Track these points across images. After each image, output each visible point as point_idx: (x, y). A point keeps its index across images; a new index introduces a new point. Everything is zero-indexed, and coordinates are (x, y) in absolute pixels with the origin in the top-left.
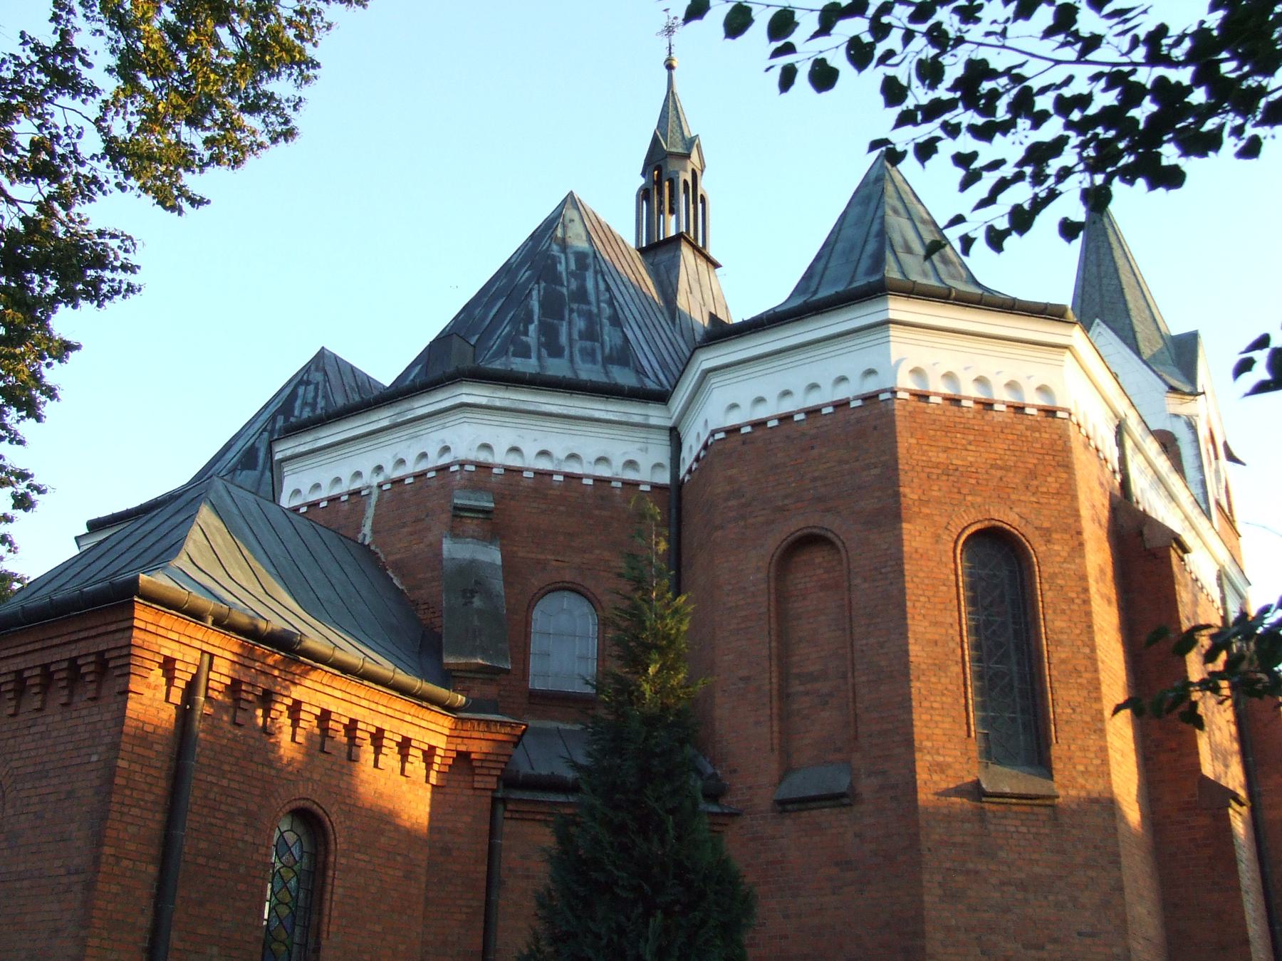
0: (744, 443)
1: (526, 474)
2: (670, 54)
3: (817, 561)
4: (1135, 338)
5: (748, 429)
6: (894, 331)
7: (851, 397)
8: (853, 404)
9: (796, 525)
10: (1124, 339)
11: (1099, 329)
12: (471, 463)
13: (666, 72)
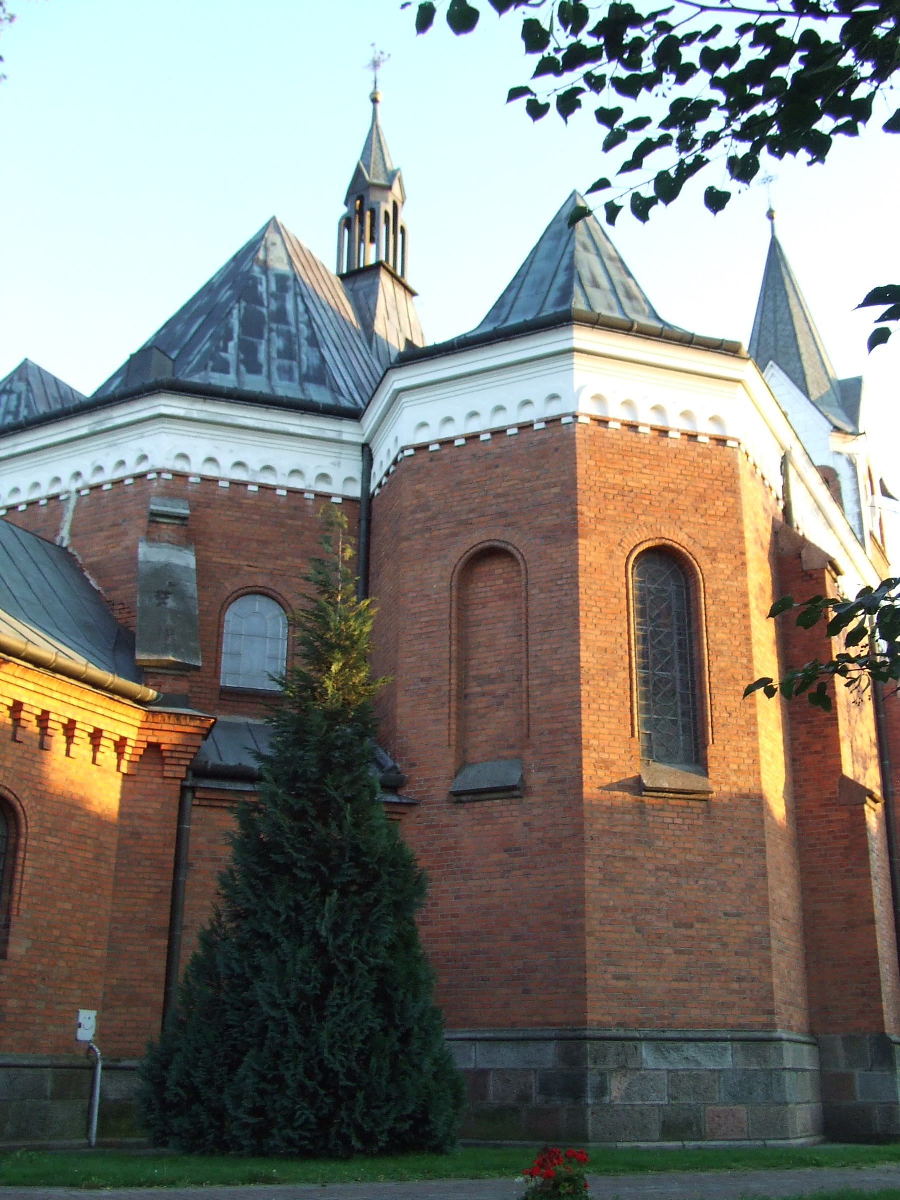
2: (376, 87)
4: (805, 379)
6: (578, 359)
7: (535, 420)
10: (795, 381)
11: (772, 371)
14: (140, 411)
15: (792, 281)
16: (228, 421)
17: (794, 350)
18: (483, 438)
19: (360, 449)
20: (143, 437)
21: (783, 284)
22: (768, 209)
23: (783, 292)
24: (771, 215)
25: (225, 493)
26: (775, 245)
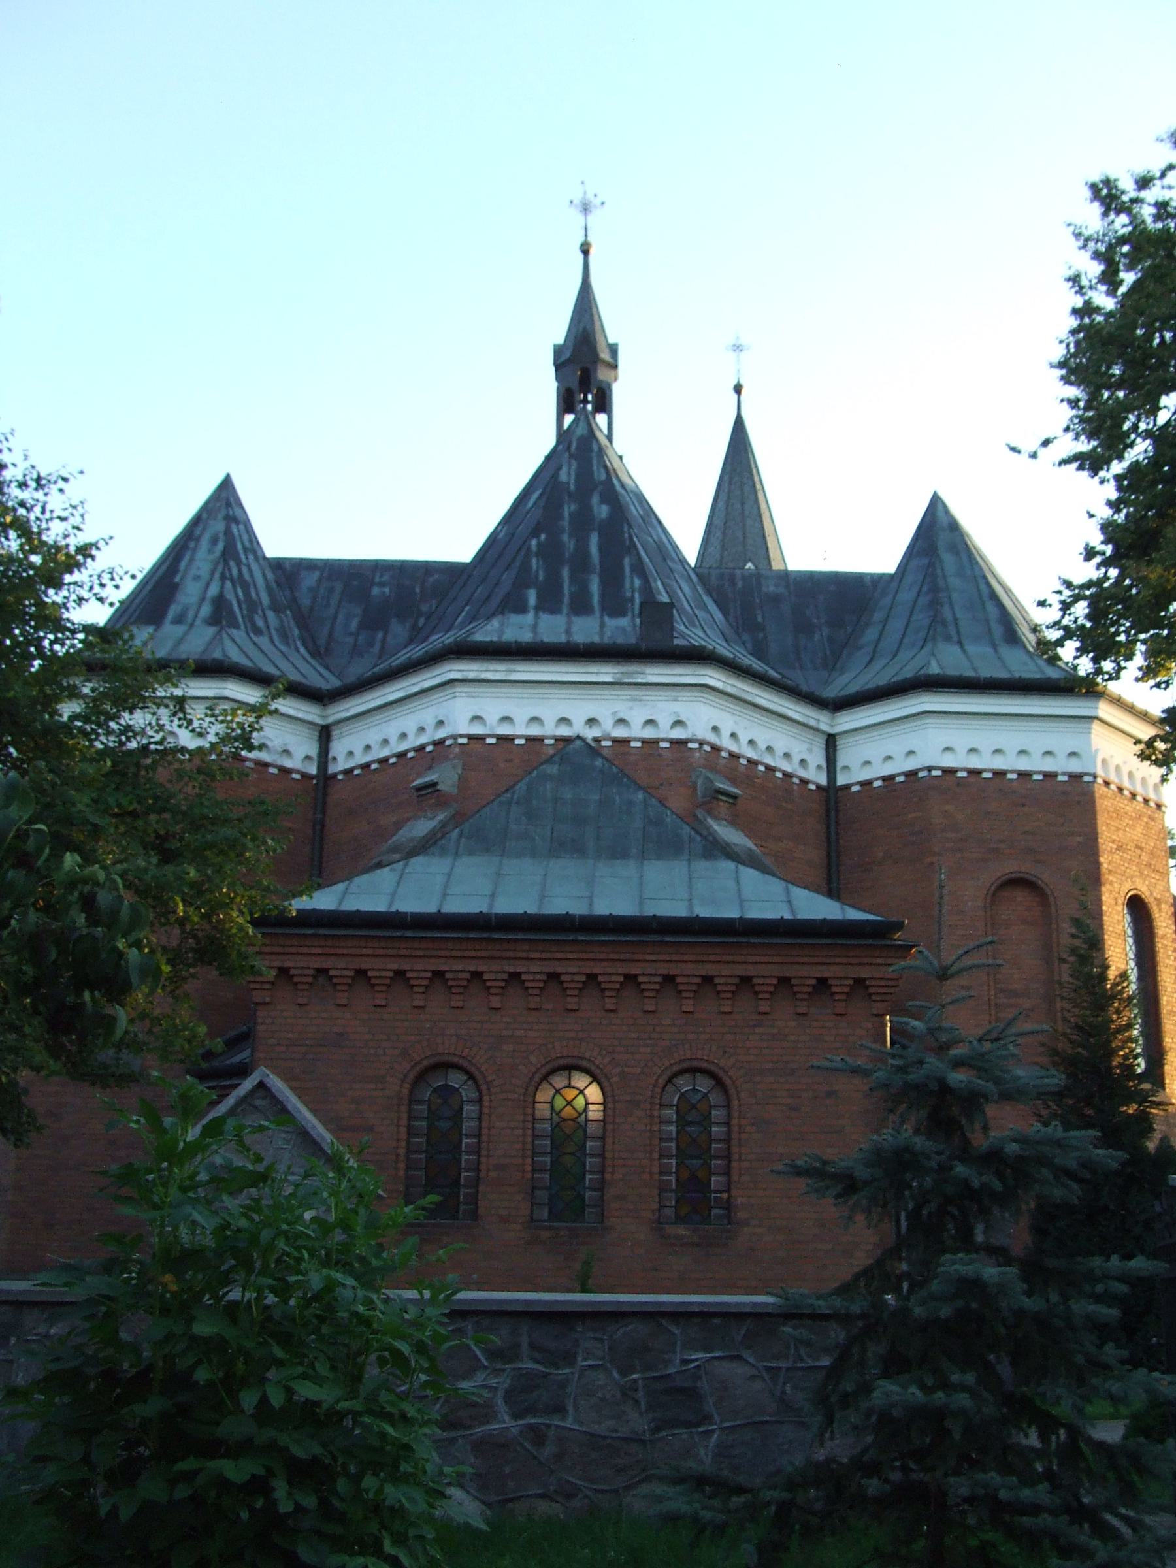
0: (958, 785)
1: (633, 744)
2: (586, 235)
3: (1019, 899)
5: (964, 774)
6: (1096, 726)
7: (1060, 771)
8: (1060, 778)
9: (1026, 868)
12: (708, 743)
13: (581, 257)
14: (680, 675)
15: (995, 575)
16: (750, 698)
17: (764, 552)
18: (1010, 776)
19: (826, 737)
20: (676, 700)
21: (752, 475)
22: (735, 382)
23: (751, 483)
24: (738, 389)
25: (742, 769)
26: (739, 427)
